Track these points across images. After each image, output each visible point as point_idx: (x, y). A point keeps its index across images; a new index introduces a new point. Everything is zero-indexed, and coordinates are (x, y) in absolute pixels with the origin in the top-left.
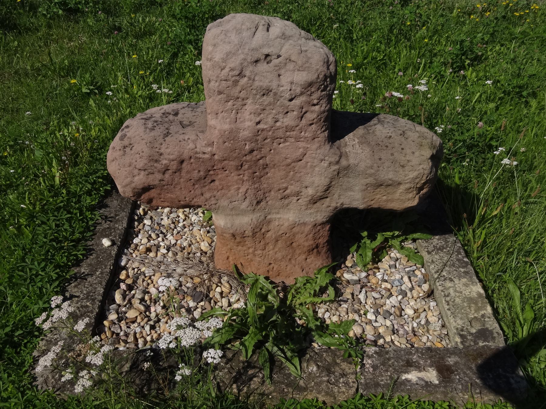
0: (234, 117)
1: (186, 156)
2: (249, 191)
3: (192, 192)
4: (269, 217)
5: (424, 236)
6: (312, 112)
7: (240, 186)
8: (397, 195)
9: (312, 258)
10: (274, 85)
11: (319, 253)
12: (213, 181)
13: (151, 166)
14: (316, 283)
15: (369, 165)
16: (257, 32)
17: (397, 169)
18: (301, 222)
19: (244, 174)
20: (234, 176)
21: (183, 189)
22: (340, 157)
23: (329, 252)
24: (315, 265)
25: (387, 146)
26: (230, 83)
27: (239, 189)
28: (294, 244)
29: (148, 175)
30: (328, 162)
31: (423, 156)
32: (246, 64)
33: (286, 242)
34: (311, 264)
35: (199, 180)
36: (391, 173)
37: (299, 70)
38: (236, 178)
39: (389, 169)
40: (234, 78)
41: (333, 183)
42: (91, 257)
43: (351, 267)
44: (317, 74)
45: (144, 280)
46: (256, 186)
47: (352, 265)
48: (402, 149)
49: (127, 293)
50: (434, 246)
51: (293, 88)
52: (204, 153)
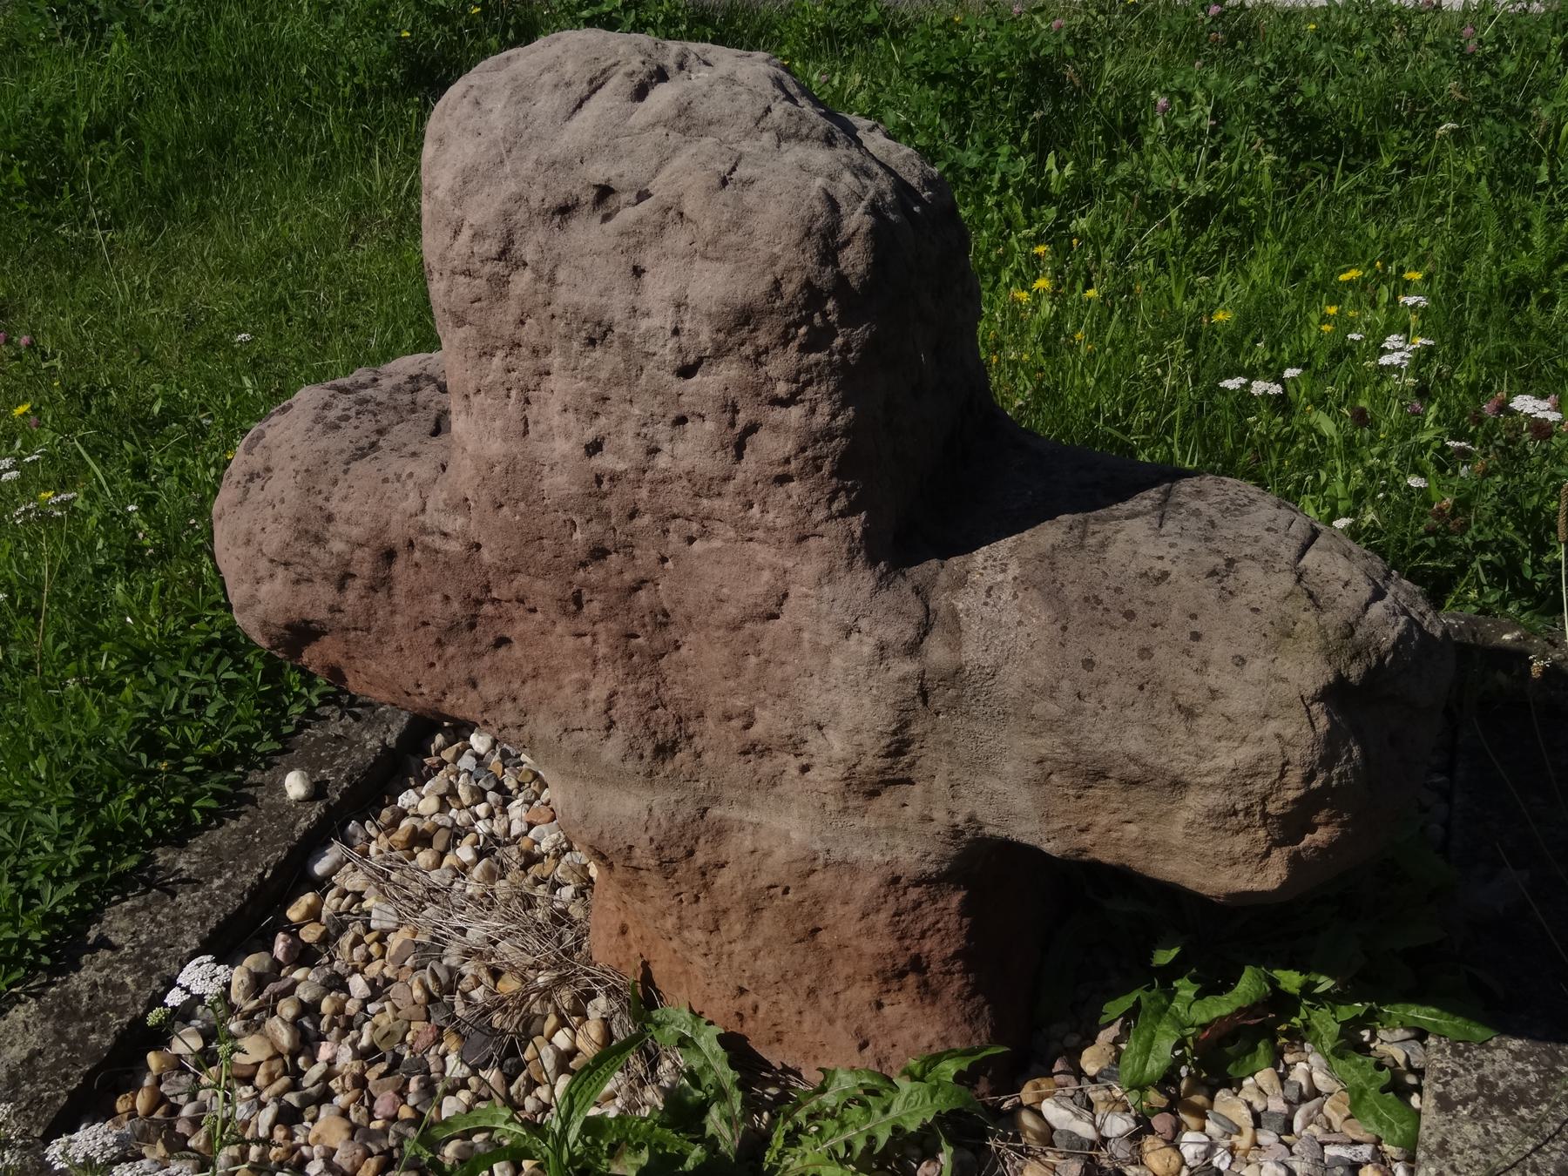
0: (517, 416)
1: (395, 535)
2: (621, 702)
3: (438, 668)
4: (716, 812)
5: (1451, 1024)
6: (775, 428)
7: (589, 676)
8: (1176, 832)
9: (898, 1007)
10: (617, 313)
11: (928, 993)
12: (502, 642)
13: (303, 555)
14: (886, 1111)
15: (1039, 681)
16: (595, 98)
17: (1164, 720)
18: (837, 855)
19: (594, 635)
20: (562, 640)
21: (407, 652)
22: (925, 629)
23: (980, 999)
24: (916, 1037)
25: (1130, 615)
26: (480, 285)
27: (585, 686)
28: (823, 937)
29: (297, 582)
30: (871, 641)
31: (1285, 680)
32: (521, 216)
33: (789, 923)
34: (899, 1028)
35: (453, 628)
36: (1137, 731)
37: (704, 257)
38: (570, 642)
39: (1128, 712)
40: (488, 269)
41: (915, 729)
42: (233, 825)
43: (1093, 1080)
44: (769, 278)
45: (358, 941)
46: (644, 685)
47: (1100, 1073)
48: (1196, 636)
49: (283, 972)
50: (1482, 1081)
51: (687, 325)
52: (445, 535)
